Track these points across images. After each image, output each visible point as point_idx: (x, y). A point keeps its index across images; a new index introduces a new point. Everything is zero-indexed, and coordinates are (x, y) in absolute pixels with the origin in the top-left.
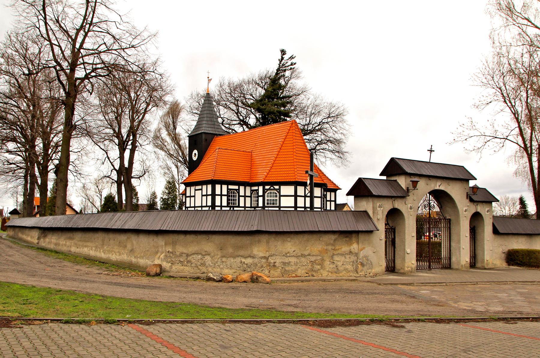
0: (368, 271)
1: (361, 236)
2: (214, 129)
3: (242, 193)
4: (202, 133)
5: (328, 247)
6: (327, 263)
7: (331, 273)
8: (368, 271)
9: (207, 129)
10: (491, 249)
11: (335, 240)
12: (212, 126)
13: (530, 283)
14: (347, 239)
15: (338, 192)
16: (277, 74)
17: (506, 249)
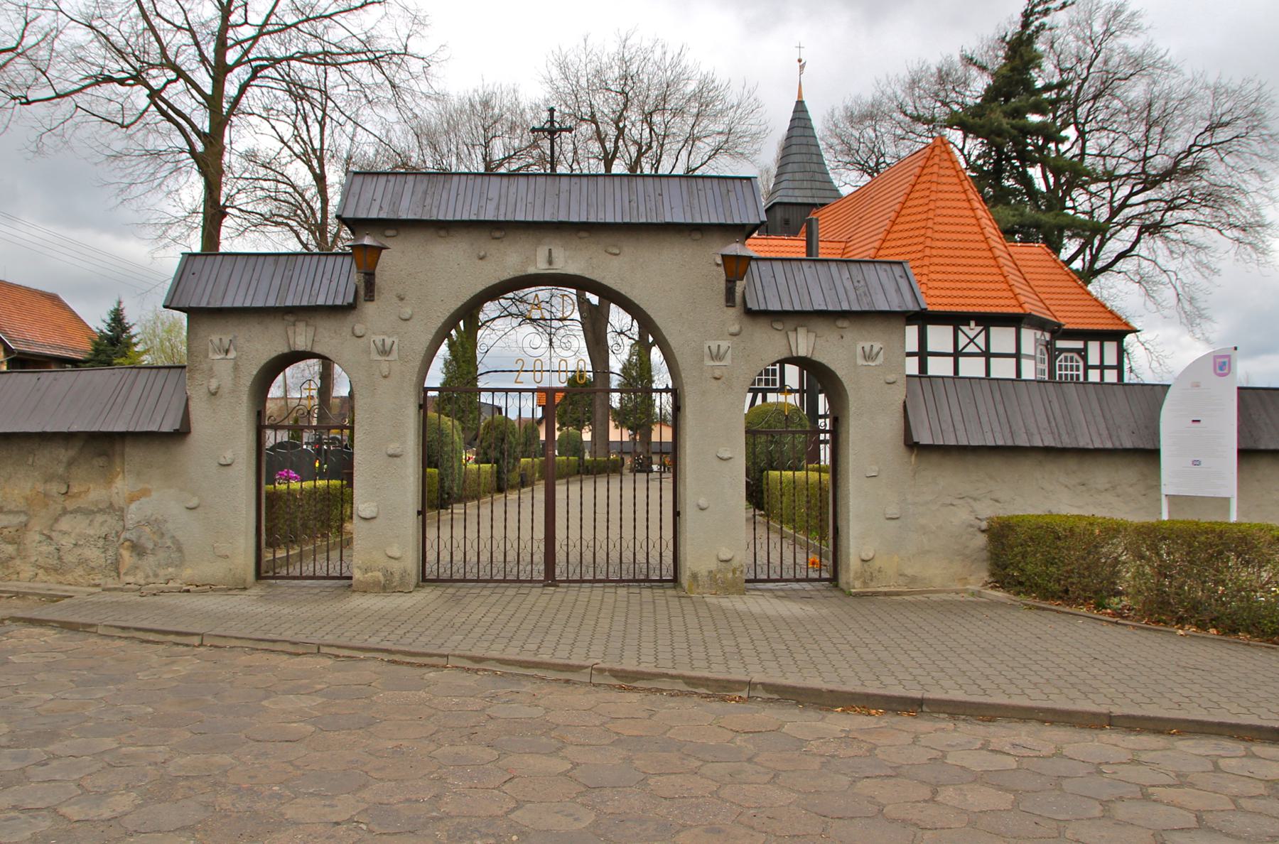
0: (162, 572)
1: (134, 455)
2: (809, 193)
3: (1093, 359)
4: (774, 204)
5: (48, 486)
6: (33, 537)
7: (46, 570)
8: (162, 572)
9: (790, 193)
10: (893, 510)
11: (70, 464)
12: (805, 184)
13: (551, 675)
14: (100, 461)
15: (1129, 339)
16: (1025, 25)
17: (988, 511)
